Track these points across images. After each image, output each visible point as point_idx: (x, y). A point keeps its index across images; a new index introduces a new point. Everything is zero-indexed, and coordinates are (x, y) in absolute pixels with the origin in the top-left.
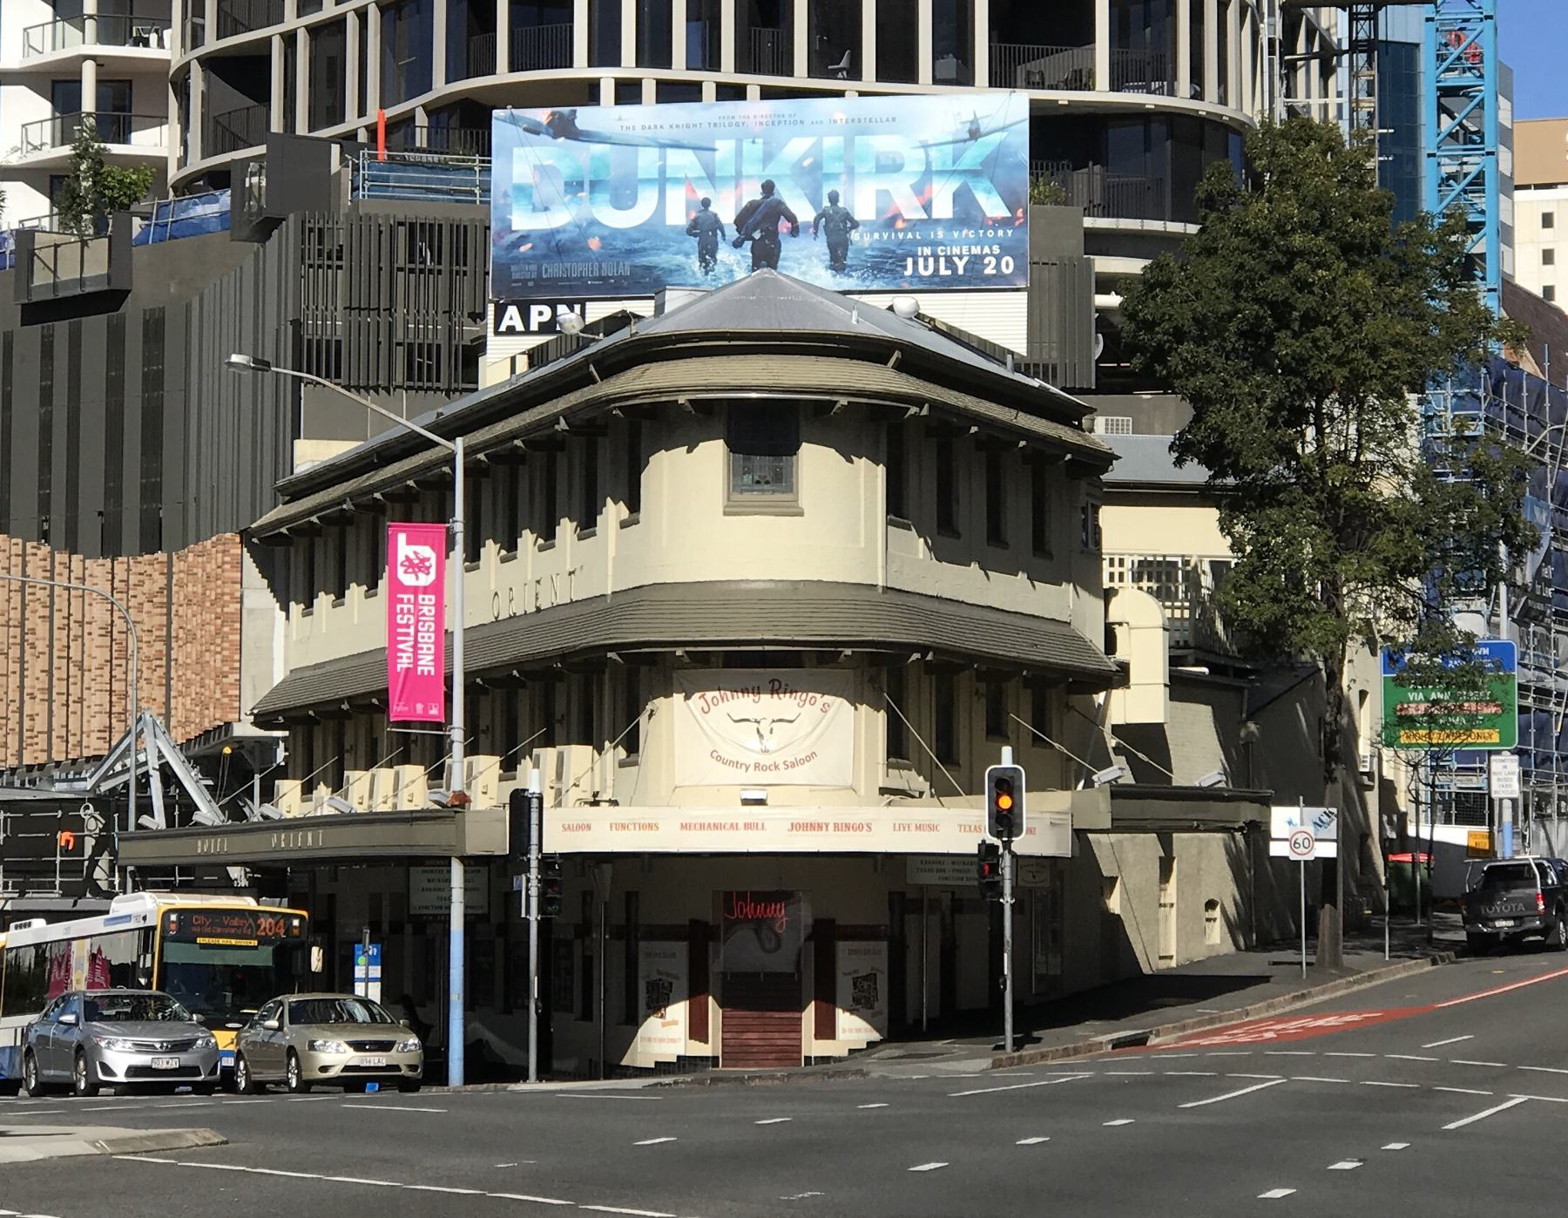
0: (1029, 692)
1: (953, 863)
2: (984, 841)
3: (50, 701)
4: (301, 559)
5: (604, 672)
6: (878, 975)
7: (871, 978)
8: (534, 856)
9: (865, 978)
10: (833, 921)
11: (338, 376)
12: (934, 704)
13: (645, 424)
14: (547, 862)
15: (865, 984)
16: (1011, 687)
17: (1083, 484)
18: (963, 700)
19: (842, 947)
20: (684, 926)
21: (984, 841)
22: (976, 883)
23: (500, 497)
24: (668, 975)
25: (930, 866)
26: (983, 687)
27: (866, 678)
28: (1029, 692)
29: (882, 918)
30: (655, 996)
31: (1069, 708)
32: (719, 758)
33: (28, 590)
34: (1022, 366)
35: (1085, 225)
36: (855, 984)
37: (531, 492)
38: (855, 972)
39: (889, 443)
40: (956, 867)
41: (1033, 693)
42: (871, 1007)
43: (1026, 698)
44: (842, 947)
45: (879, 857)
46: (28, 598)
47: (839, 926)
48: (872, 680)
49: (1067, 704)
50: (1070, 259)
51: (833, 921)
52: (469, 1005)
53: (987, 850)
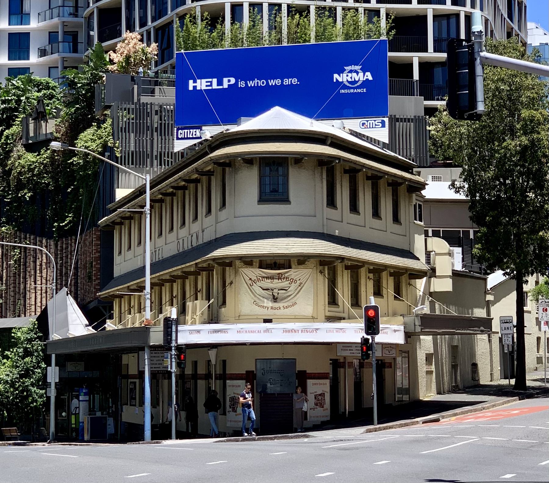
0: (392, 278)
1: (356, 347)
2: (363, 337)
3: (36, 293)
4: (118, 234)
5: (213, 270)
6: (326, 393)
7: (323, 395)
8: (174, 344)
9: (320, 395)
10: (306, 371)
11: (125, 164)
12: (349, 282)
13: (227, 169)
14: (180, 349)
15: (320, 398)
16: (384, 274)
17: (414, 195)
18: (363, 281)
19: (310, 382)
20: (244, 374)
21: (363, 337)
22: (360, 355)
23: (180, 204)
24: (238, 394)
25: (347, 348)
26: (371, 275)
27: (318, 271)
28: (392, 278)
29: (328, 369)
30: (232, 403)
31: (410, 284)
32: (257, 304)
33: (28, 251)
34: (384, 145)
35: (424, 104)
36: (315, 398)
37: (190, 202)
38: (315, 392)
39: (327, 176)
40: (357, 348)
41: (394, 279)
42: (323, 407)
43: (391, 281)
44: (310, 382)
45: (339, 347)
46: (27, 254)
47: (308, 373)
48: (321, 272)
49: (409, 283)
50: (419, 117)
51: (306, 371)
52: (372, 408)
53: (365, 341)
